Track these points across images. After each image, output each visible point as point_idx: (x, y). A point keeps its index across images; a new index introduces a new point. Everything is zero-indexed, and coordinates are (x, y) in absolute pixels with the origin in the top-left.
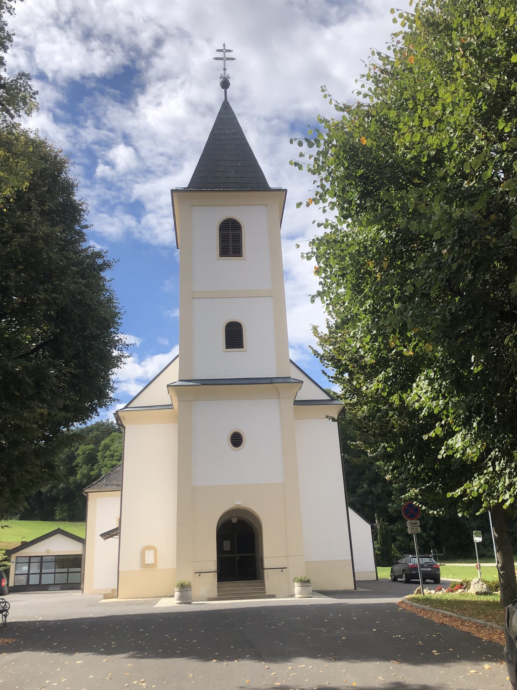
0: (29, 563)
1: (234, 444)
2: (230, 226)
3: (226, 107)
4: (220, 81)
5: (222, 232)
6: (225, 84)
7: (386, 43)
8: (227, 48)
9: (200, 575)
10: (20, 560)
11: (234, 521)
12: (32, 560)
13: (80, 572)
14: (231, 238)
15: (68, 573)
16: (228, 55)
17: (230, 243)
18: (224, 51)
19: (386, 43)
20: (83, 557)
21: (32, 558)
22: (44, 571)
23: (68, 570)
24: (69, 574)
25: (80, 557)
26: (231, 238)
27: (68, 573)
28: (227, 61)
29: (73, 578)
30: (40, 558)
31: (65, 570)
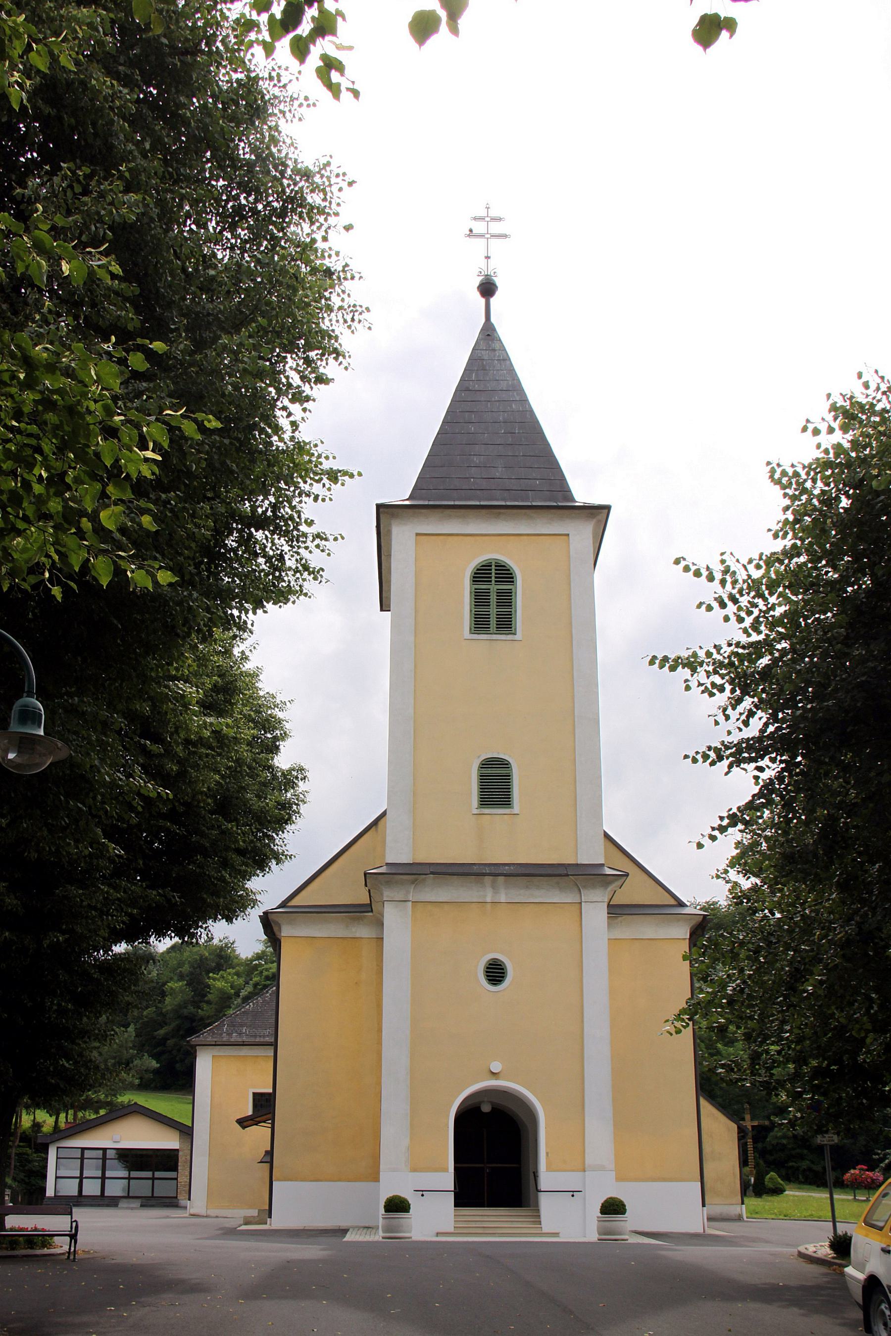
0: (82, 1158)
1: (489, 980)
2: (493, 571)
3: (488, 332)
4: (477, 281)
5: (477, 587)
6: (487, 289)
7: (709, 716)
8: (493, 213)
9: (423, 1195)
10: (62, 1153)
11: (486, 1108)
12: (87, 1154)
13: (176, 1179)
14: (493, 598)
15: (153, 1179)
16: (495, 228)
17: (491, 606)
18: (488, 236)
19: (709, 716)
20: (742, 1165)
21: (86, 1151)
22: (108, 1174)
23: (153, 1174)
24: (156, 1181)
25: (176, 1152)
26: (493, 598)
27: (129, 1178)
28: (493, 241)
29: (163, 1189)
30: (101, 1152)
31: (149, 1174)
